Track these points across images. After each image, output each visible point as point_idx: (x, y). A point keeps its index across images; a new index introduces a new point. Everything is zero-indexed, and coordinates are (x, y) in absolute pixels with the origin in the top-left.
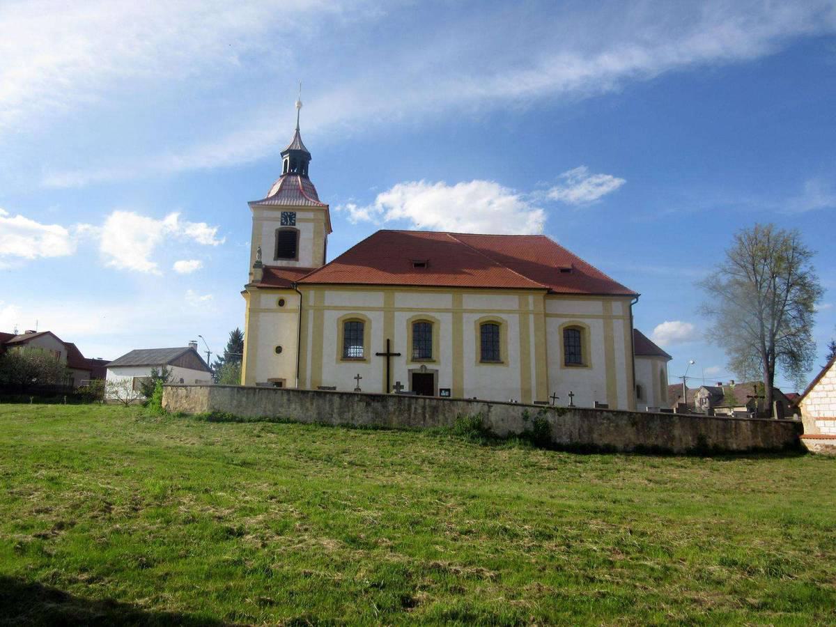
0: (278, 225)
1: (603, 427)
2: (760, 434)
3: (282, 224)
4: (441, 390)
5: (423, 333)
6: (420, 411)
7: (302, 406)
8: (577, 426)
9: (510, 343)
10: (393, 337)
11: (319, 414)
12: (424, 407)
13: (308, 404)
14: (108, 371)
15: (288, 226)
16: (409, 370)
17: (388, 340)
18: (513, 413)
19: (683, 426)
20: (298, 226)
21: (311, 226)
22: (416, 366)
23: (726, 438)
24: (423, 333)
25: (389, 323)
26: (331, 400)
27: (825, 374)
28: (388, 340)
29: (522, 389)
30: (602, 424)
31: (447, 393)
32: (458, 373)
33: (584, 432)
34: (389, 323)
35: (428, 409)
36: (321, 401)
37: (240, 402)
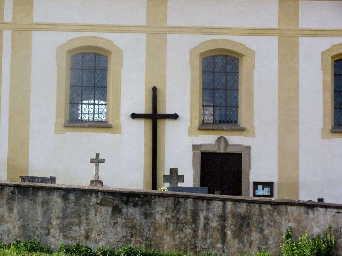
4: (256, 184)
6: (214, 224)
11: (24, 227)
12: (223, 218)
16: (195, 147)
17: (155, 90)
22: (209, 140)
25: (156, 58)
26: (45, 203)
28: (155, 90)
31: (267, 191)
32: (288, 154)
34: (156, 58)
35: (230, 221)
36: (27, 204)
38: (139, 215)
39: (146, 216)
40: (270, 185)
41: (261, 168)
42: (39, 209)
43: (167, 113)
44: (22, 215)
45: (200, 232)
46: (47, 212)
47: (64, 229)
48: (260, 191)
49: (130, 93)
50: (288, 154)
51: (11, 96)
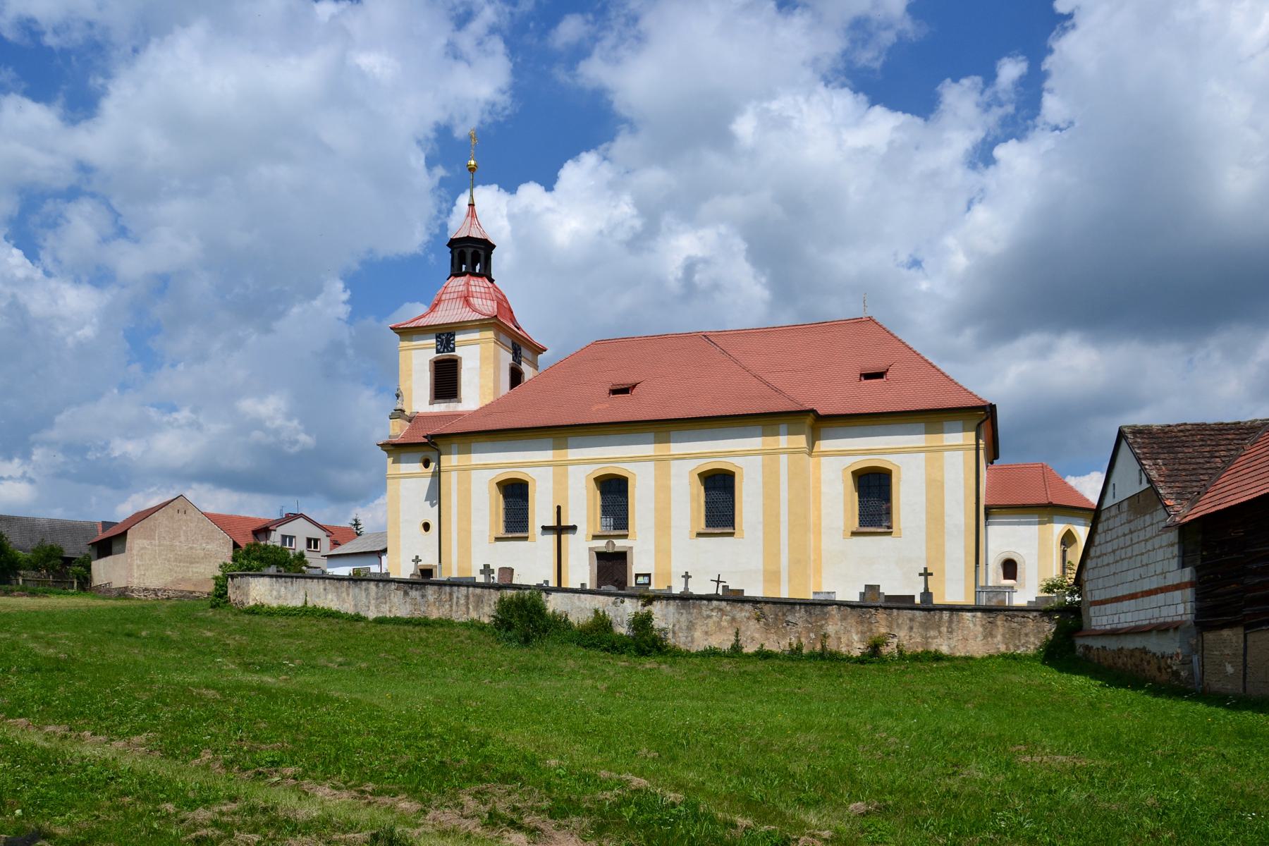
0: (433, 354)
1: (710, 622)
2: (1001, 630)
3: (438, 352)
4: (637, 576)
5: (613, 491)
6: (462, 601)
7: (338, 596)
8: (671, 621)
9: (907, 497)
10: (566, 498)
11: (356, 605)
12: (467, 597)
13: (344, 595)
14: (1189, 618)
15: (446, 355)
16: (590, 549)
17: (559, 508)
18: (577, 603)
19: (844, 618)
20: (459, 352)
21: (476, 349)
22: (601, 545)
23: (927, 638)
24: (613, 491)
25: (560, 484)
26: (367, 589)
27: (820, 492)
28: (559, 508)
29: (765, 571)
30: (709, 617)
31: (646, 580)
32: (663, 552)
33: (680, 628)
34: (560, 484)
35: (471, 599)
36: (357, 590)
37: (279, 591)
38: (518, 598)
39: (423, 596)
40: (649, 575)
41: (639, 564)
42: (364, 594)
43: (1037, 527)
44: (355, 598)
45: (454, 607)
46: (368, 595)
47: (377, 607)
48: (641, 580)
49: (540, 513)
50: (663, 552)
51: (779, 521)
